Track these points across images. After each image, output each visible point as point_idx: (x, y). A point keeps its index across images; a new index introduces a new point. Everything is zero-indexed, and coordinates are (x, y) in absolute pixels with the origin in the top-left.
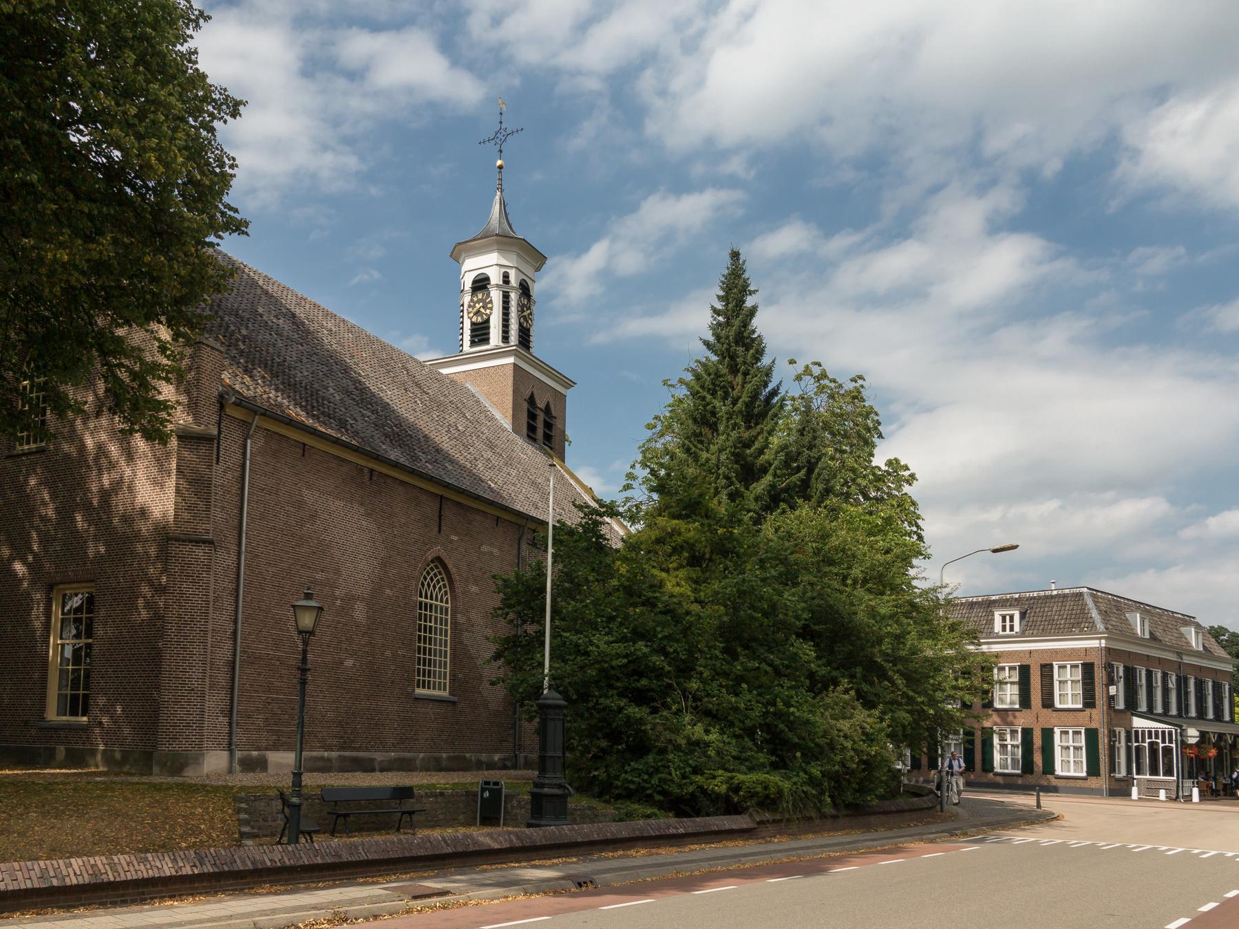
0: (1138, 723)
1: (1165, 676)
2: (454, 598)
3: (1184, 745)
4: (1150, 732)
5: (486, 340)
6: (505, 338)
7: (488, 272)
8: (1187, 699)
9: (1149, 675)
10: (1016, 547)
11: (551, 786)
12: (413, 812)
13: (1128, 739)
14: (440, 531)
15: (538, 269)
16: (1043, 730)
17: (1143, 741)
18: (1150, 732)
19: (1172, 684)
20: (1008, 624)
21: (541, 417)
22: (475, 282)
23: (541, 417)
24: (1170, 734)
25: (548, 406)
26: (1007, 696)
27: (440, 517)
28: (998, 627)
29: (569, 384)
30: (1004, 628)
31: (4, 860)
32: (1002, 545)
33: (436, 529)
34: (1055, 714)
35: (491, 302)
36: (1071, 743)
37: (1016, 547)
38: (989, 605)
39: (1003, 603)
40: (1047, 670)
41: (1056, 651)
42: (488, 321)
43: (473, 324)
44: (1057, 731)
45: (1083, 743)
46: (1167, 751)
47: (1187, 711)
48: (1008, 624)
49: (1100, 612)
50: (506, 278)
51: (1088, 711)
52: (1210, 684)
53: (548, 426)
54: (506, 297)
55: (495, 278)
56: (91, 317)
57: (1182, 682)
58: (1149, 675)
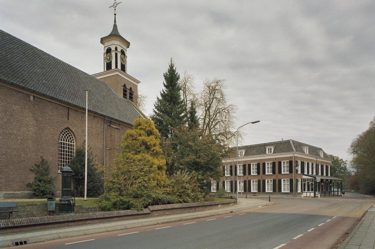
0: (304, 177)
1: (312, 164)
4: (307, 179)
8: (318, 170)
9: (308, 164)
10: (259, 121)
13: (302, 181)
14: (68, 119)
16: (249, 180)
19: (314, 167)
20: (270, 151)
21: (128, 92)
23: (128, 92)
24: (313, 180)
25: (131, 88)
27: (68, 114)
28: (267, 152)
29: (138, 82)
30: (269, 152)
31: (1, 219)
33: (67, 119)
35: (112, 56)
37: (259, 121)
39: (269, 144)
40: (280, 163)
41: (282, 158)
42: (111, 62)
43: (107, 63)
44: (252, 181)
47: (318, 174)
48: (270, 151)
49: (295, 146)
50: (116, 49)
52: (325, 166)
53: (131, 94)
54: (116, 54)
55: (113, 48)
56: (185, 127)
57: (322, 166)
58: (308, 164)
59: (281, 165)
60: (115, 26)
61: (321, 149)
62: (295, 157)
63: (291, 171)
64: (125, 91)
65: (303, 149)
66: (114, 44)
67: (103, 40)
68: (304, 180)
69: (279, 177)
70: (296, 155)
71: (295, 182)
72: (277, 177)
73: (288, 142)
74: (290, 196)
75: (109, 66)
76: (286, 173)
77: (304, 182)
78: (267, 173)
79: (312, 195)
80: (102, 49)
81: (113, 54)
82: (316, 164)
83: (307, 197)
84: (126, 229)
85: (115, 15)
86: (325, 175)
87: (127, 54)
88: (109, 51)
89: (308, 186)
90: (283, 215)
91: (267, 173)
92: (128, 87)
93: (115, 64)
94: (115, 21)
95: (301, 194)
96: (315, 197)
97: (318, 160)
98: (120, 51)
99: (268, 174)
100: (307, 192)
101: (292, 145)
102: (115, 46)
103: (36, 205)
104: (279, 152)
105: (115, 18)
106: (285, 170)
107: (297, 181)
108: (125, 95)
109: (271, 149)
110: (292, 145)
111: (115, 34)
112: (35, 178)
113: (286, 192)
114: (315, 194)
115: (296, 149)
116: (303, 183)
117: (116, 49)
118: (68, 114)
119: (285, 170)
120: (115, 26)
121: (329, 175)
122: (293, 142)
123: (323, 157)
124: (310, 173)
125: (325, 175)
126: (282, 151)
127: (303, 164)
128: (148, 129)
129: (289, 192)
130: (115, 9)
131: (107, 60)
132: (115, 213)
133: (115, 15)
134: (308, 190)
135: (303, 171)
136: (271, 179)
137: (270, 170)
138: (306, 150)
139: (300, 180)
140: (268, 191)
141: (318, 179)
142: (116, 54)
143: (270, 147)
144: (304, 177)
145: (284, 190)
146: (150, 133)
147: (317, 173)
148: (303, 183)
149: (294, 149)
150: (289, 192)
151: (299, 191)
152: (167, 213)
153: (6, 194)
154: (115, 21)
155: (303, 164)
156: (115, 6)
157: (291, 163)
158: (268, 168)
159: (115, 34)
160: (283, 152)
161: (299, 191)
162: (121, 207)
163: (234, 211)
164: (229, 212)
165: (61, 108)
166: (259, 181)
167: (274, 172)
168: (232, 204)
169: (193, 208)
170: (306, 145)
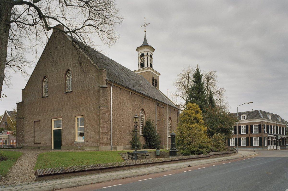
0: (269, 136)
1: (274, 127)
2: (145, 116)
3: (277, 139)
4: (271, 137)
5: (144, 67)
6: (148, 66)
7: (144, 53)
9: (271, 126)
10: (253, 102)
11: (174, 150)
12: (148, 155)
13: (267, 139)
15: (153, 52)
17: (270, 139)
18: (271, 137)
19: (275, 128)
22: (141, 55)
25: (156, 79)
26: (243, 132)
27: (143, 101)
28: (242, 119)
29: (160, 74)
30: (243, 119)
32: (250, 102)
34: (253, 135)
35: (145, 59)
36: (256, 140)
37: (253, 102)
38: (240, 114)
40: (251, 127)
41: (253, 123)
43: (141, 63)
44: (253, 138)
45: (259, 140)
46: (274, 141)
47: (278, 133)
48: (244, 118)
50: (147, 54)
51: (260, 134)
53: (156, 83)
54: (147, 58)
55: (145, 54)
57: (277, 128)
58: (271, 126)
59: (241, 128)
60: (145, 39)
61: (278, 116)
62: (263, 122)
63: (260, 132)
64: (153, 81)
65: (268, 116)
66: (145, 51)
67: (137, 49)
68: (269, 137)
69: (251, 135)
70: (263, 121)
71: (263, 139)
72: (250, 135)
73: (257, 112)
74: (259, 149)
75: (142, 65)
76: (244, 133)
77: (269, 139)
78: (242, 133)
79: (275, 148)
80: (137, 55)
81: (146, 57)
82: (276, 126)
83: (271, 149)
84: (164, 171)
85: (145, 31)
86: (282, 134)
87: (153, 56)
88: (142, 55)
89: (272, 141)
90: (272, 158)
91: (242, 133)
92: (155, 79)
93: (147, 64)
94: (145, 36)
95: (267, 147)
96: (277, 149)
97: (278, 123)
98: (150, 55)
99: (242, 134)
100: (271, 146)
101: (260, 113)
102: (145, 53)
103: (152, 152)
104: (251, 119)
105: (145, 34)
106: (255, 131)
107: (264, 138)
108: (153, 83)
109: (245, 117)
110: (260, 113)
111: (145, 45)
112: (132, 138)
113: (256, 146)
114: (277, 147)
115: (263, 116)
116: (268, 140)
117: (147, 54)
118: (143, 101)
119: (255, 131)
120: (145, 39)
121: (285, 134)
122: (261, 111)
123: (280, 121)
124: (273, 133)
125: (282, 134)
126: (253, 118)
127: (268, 126)
128: (196, 110)
129: (258, 146)
130: (145, 28)
131: (142, 61)
132: (194, 156)
133: (145, 31)
134: (271, 145)
135: (268, 132)
136: (245, 137)
137: (244, 131)
138: (270, 117)
139: (266, 138)
140: (232, 146)
141: (279, 137)
142: (147, 58)
143: (244, 115)
144: (269, 136)
145: (255, 145)
146: (197, 112)
147: (277, 132)
148: (268, 140)
149: (262, 116)
150: (258, 146)
151: (266, 145)
152: (215, 157)
153: (123, 147)
154: (145, 36)
155: (268, 126)
156: (145, 25)
157: (260, 126)
158: (243, 129)
159: (145, 45)
160: (254, 118)
161: (266, 145)
162: (197, 153)
163: (244, 157)
164: (187, 166)
165: (136, 96)
166: (247, 139)
167: (247, 132)
168: (233, 153)
169: (224, 155)
170: (269, 113)
